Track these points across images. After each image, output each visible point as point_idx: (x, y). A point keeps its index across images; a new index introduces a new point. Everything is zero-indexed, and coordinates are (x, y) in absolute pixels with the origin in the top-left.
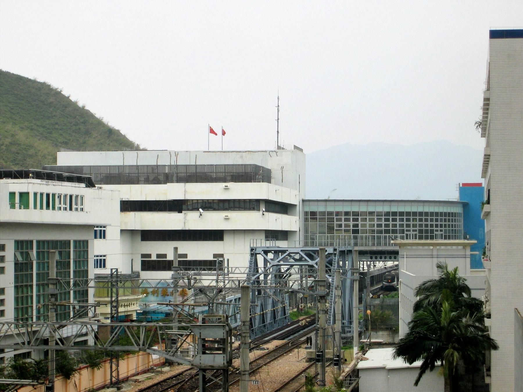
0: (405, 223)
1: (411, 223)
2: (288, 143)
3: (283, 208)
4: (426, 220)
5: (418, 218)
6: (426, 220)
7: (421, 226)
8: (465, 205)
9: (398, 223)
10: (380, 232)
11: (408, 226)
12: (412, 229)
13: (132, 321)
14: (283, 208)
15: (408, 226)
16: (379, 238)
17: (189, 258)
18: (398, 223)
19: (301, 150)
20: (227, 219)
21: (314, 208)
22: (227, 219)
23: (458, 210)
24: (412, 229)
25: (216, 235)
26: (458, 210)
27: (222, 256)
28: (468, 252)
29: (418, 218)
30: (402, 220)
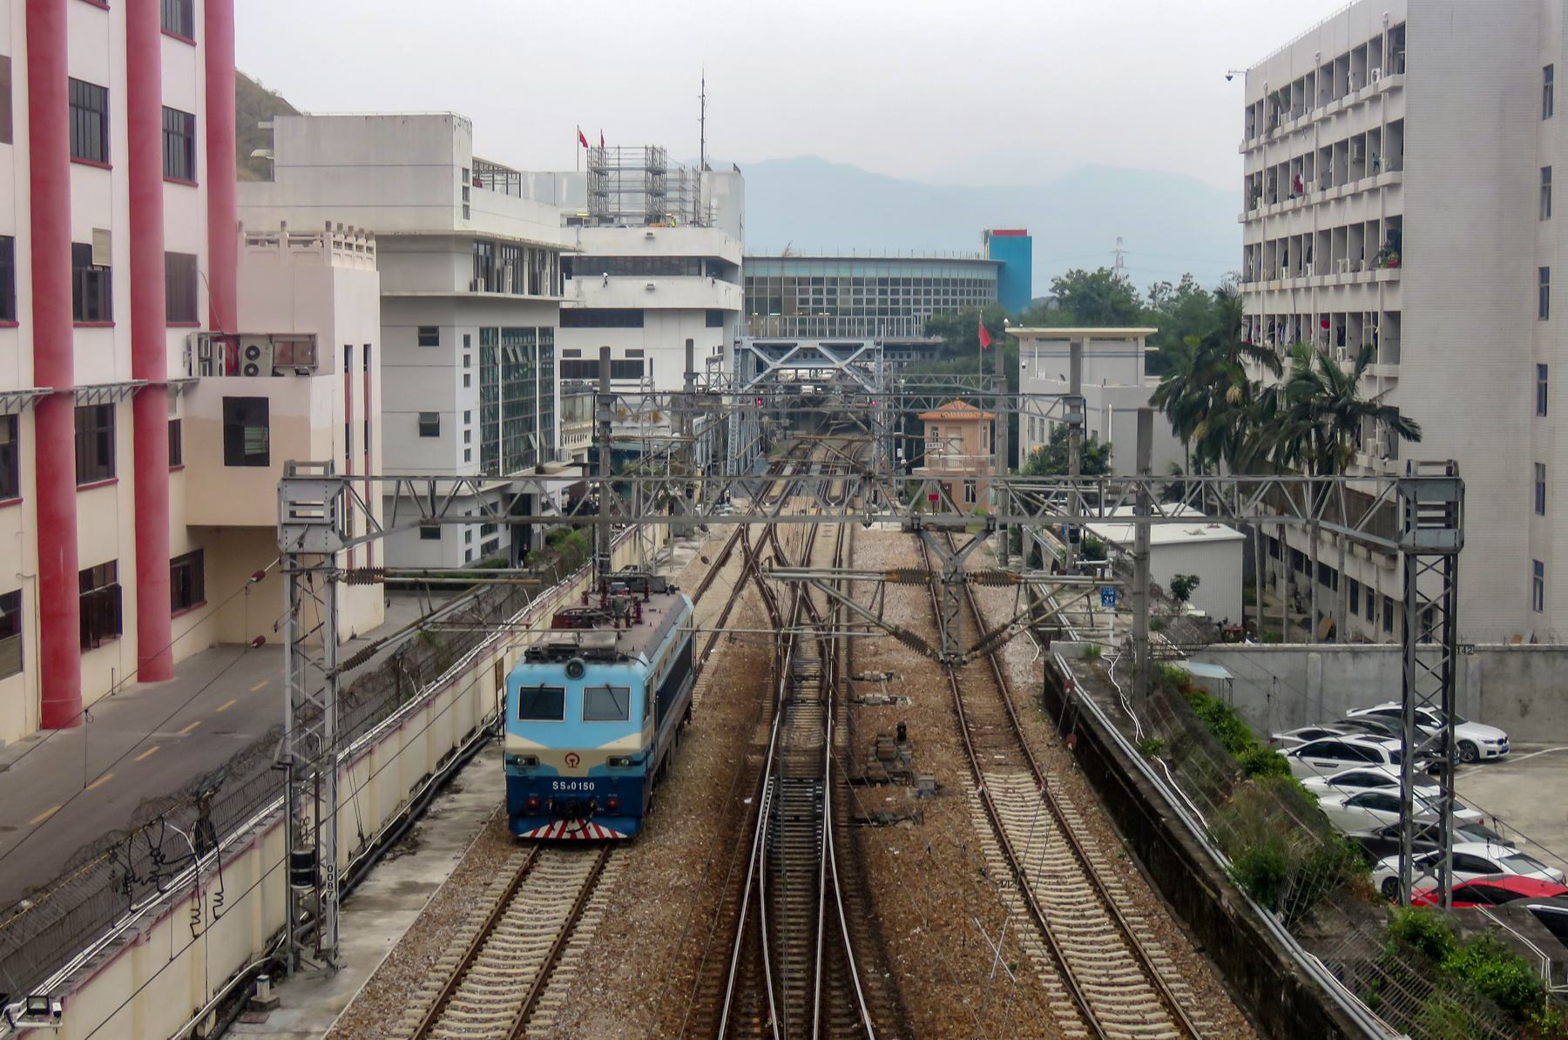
0: (912, 297)
1: (922, 297)
2: (716, 156)
3: (718, 268)
4: (946, 293)
5: (923, 288)
6: (927, 292)
7: (937, 302)
8: (1000, 267)
9: (901, 297)
10: (871, 312)
11: (917, 302)
12: (923, 307)
13: (1365, 544)
14: (718, 268)
15: (917, 302)
16: (871, 322)
17: (584, 357)
18: (901, 297)
19: (1548, 110)
20: (650, 289)
21: (759, 272)
22: (650, 289)
23: (990, 275)
24: (923, 307)
25: (631, 318)
26: (990, 275)
27: (640, 353)
28: (1143, 348)
29: (923, 288)
30: (908, 292)
